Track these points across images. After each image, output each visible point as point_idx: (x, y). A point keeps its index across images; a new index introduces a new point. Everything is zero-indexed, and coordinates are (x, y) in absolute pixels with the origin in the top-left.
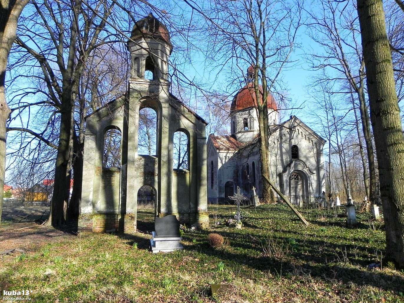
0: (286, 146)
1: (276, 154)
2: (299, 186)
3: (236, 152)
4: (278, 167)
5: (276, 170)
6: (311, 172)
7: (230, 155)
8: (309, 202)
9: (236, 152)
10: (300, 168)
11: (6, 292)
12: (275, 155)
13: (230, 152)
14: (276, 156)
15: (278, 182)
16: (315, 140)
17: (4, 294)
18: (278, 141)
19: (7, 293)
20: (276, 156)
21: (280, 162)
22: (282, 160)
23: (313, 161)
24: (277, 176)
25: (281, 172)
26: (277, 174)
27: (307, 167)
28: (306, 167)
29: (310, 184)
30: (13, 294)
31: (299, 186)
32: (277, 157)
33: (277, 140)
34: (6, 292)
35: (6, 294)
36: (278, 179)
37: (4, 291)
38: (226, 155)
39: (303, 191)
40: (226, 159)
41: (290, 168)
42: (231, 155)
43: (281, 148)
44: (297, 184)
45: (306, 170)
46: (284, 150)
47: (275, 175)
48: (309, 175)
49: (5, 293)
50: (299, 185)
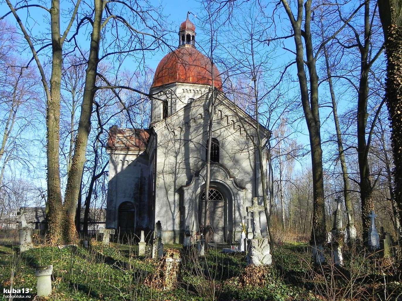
0: (196, 138)
1: (176, 153)
2: (219, 211)
3: (140, 154)
4: (179, 175)
5: (175, 182)
6: (237, 186)
7: (131, 158)
8: (233, 240)
9: (141, 152)
10: (220, 178)
11: (7, 290)
12: (175, 155)
13: (130, 153)
14: (176, 157)
15: (177, 203)
16: (251, 130)
17: (4, 292)
18: (181, 130)
19: (7, 291)
20: (176, 157)
21: (182, 166)
22: (187, 163)
23: (247, 164)
24: (176, 191)
25: (185, 184)
26: (175, 189)
27: (230, 177)
28: (228, 177)
29: (236, 209)
30: (13, 292)
31: (219, 211)
32: (179, 157)
33: (179, 129)
34: (7, 290)
35: (6, 293)
36: (177, 197)
37: (4, 289)
38: (124, 158)
39: (225, 220)
40: (123, 165)
41: (197, 178)
42: (134, 158)
43: (187, 141)
44: (215, 207)
45: (229, 182)
46: (192, 145)
47: (173, 189)
48: (235, 191)
49: (5, 291)
50: (218, 208)
